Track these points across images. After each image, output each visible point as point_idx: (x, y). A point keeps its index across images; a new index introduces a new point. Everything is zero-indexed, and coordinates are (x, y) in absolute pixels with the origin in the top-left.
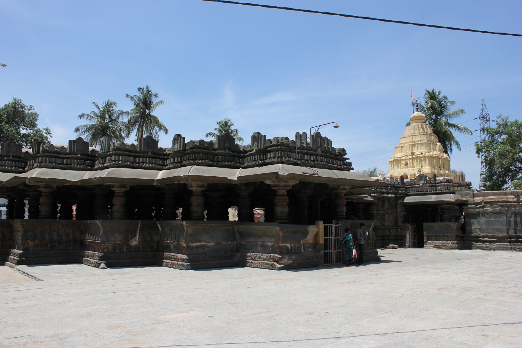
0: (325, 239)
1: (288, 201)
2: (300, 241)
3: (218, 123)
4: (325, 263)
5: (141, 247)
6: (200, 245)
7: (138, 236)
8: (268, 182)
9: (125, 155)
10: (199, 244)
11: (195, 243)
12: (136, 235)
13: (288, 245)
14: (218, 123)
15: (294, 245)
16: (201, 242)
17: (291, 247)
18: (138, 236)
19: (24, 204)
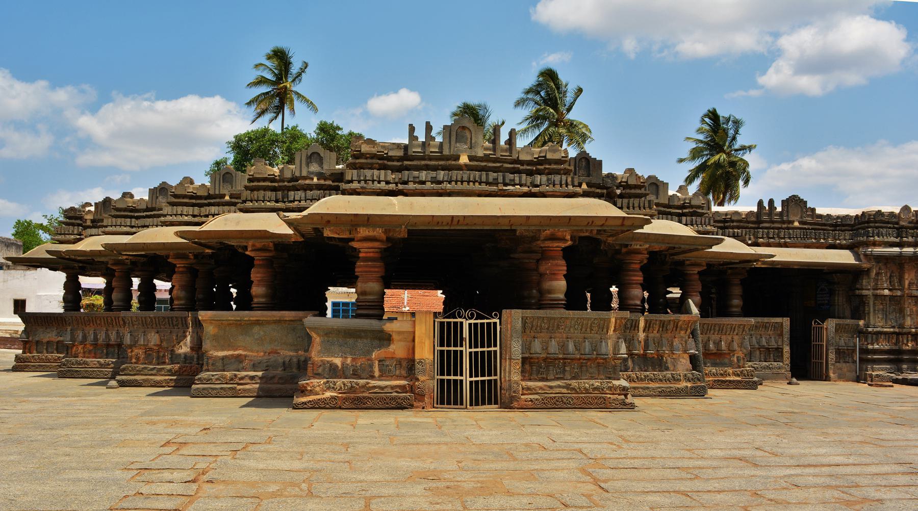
0: (442, 352)
1: (565, 268)
2: (369, 352)
3: (519, 103)
4: (442, 403)
5: (196, 356)
6: (232, 355)
7: (189, 338)
8: (327, 233)
9: (193, 205)
10: (231, 353)
11: (223, 350)
12: (185, 337)
13: (338, 361)
14: (519, 103)
15: (353, 360)
16: (236, 350)
17: (343, 364)
18: (189, 338)
19: (610, 294)
